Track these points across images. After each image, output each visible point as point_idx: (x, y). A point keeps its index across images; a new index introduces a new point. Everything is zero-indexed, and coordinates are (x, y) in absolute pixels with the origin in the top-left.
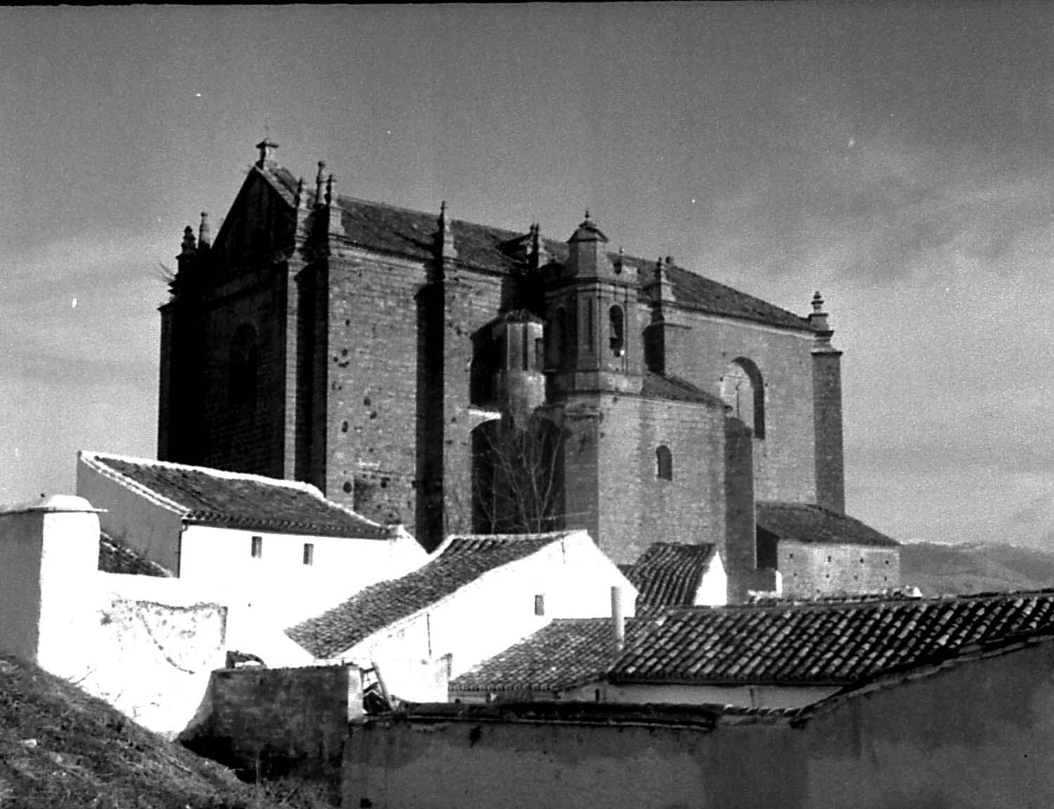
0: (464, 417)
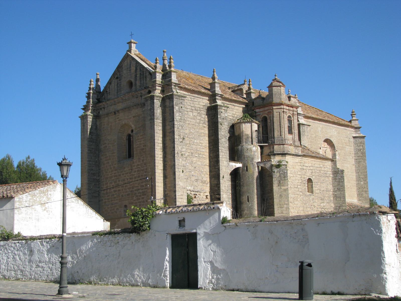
0: (227, 166)
